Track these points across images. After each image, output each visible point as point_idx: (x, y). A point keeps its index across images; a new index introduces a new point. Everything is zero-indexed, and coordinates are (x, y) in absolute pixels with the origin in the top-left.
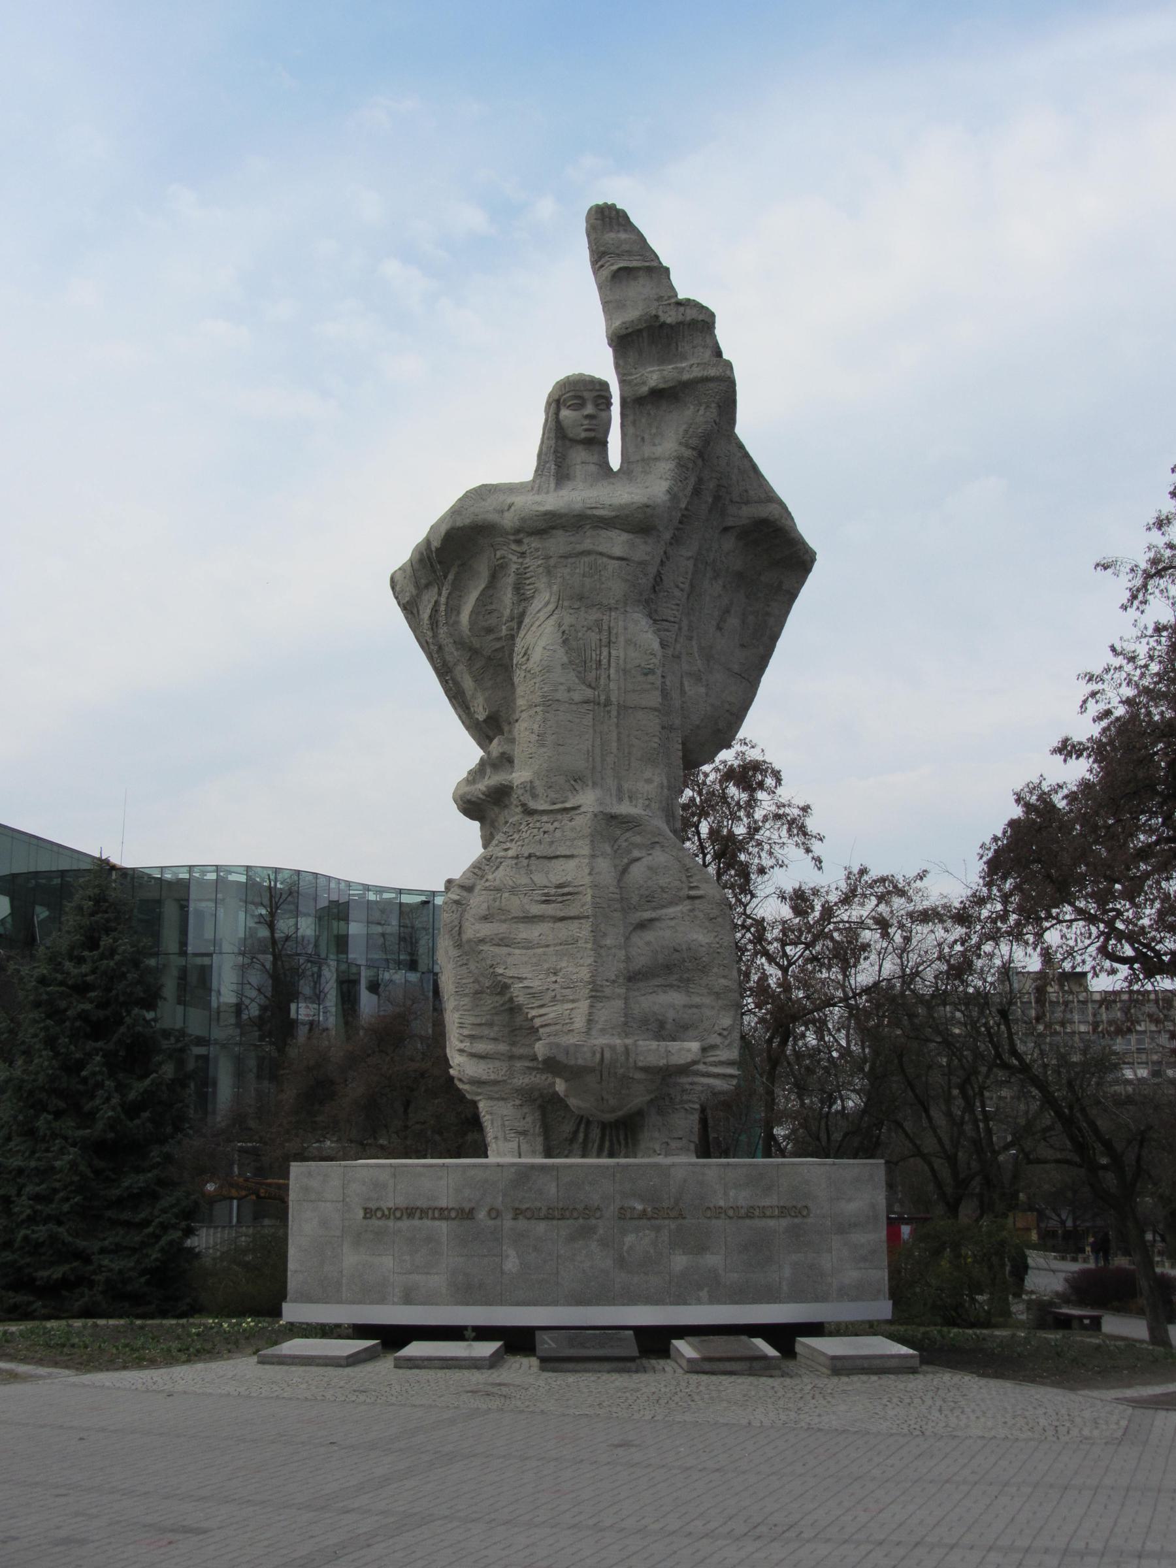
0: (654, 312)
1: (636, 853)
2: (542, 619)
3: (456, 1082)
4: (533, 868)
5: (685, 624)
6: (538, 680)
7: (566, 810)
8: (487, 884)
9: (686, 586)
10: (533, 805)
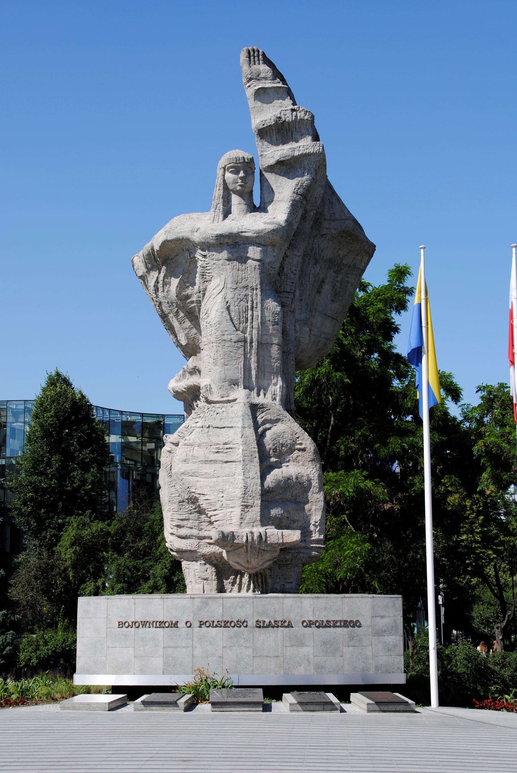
0: (279, 115)
1: (267, 426)
2: (216, 294)
3: (169, 550)
4: (210, 433)
5: (297, 294)
6: (213, 328)
7: (229, 401)
8: (186, 442)
9: (297, 272)
10: (210, 398)
